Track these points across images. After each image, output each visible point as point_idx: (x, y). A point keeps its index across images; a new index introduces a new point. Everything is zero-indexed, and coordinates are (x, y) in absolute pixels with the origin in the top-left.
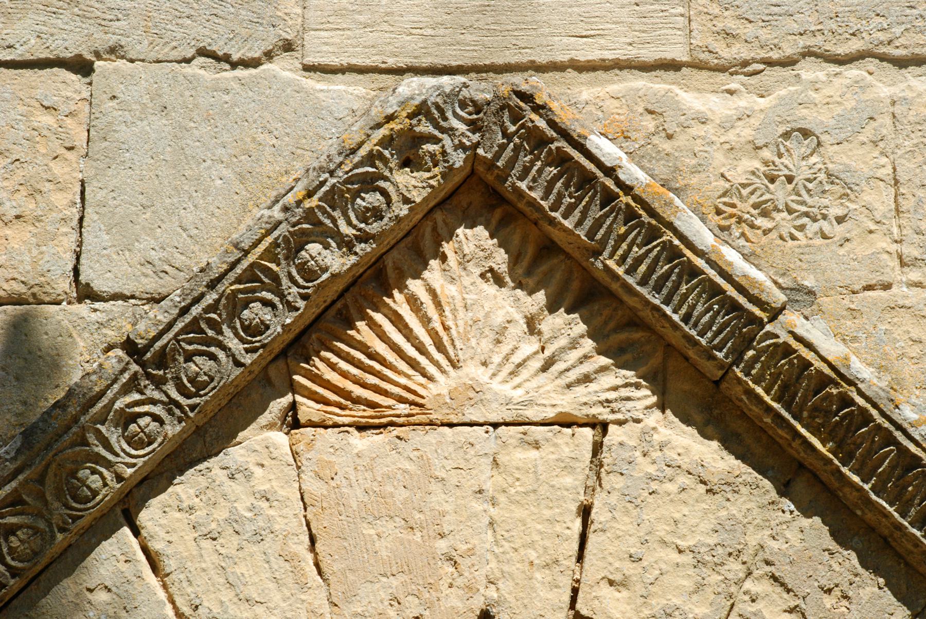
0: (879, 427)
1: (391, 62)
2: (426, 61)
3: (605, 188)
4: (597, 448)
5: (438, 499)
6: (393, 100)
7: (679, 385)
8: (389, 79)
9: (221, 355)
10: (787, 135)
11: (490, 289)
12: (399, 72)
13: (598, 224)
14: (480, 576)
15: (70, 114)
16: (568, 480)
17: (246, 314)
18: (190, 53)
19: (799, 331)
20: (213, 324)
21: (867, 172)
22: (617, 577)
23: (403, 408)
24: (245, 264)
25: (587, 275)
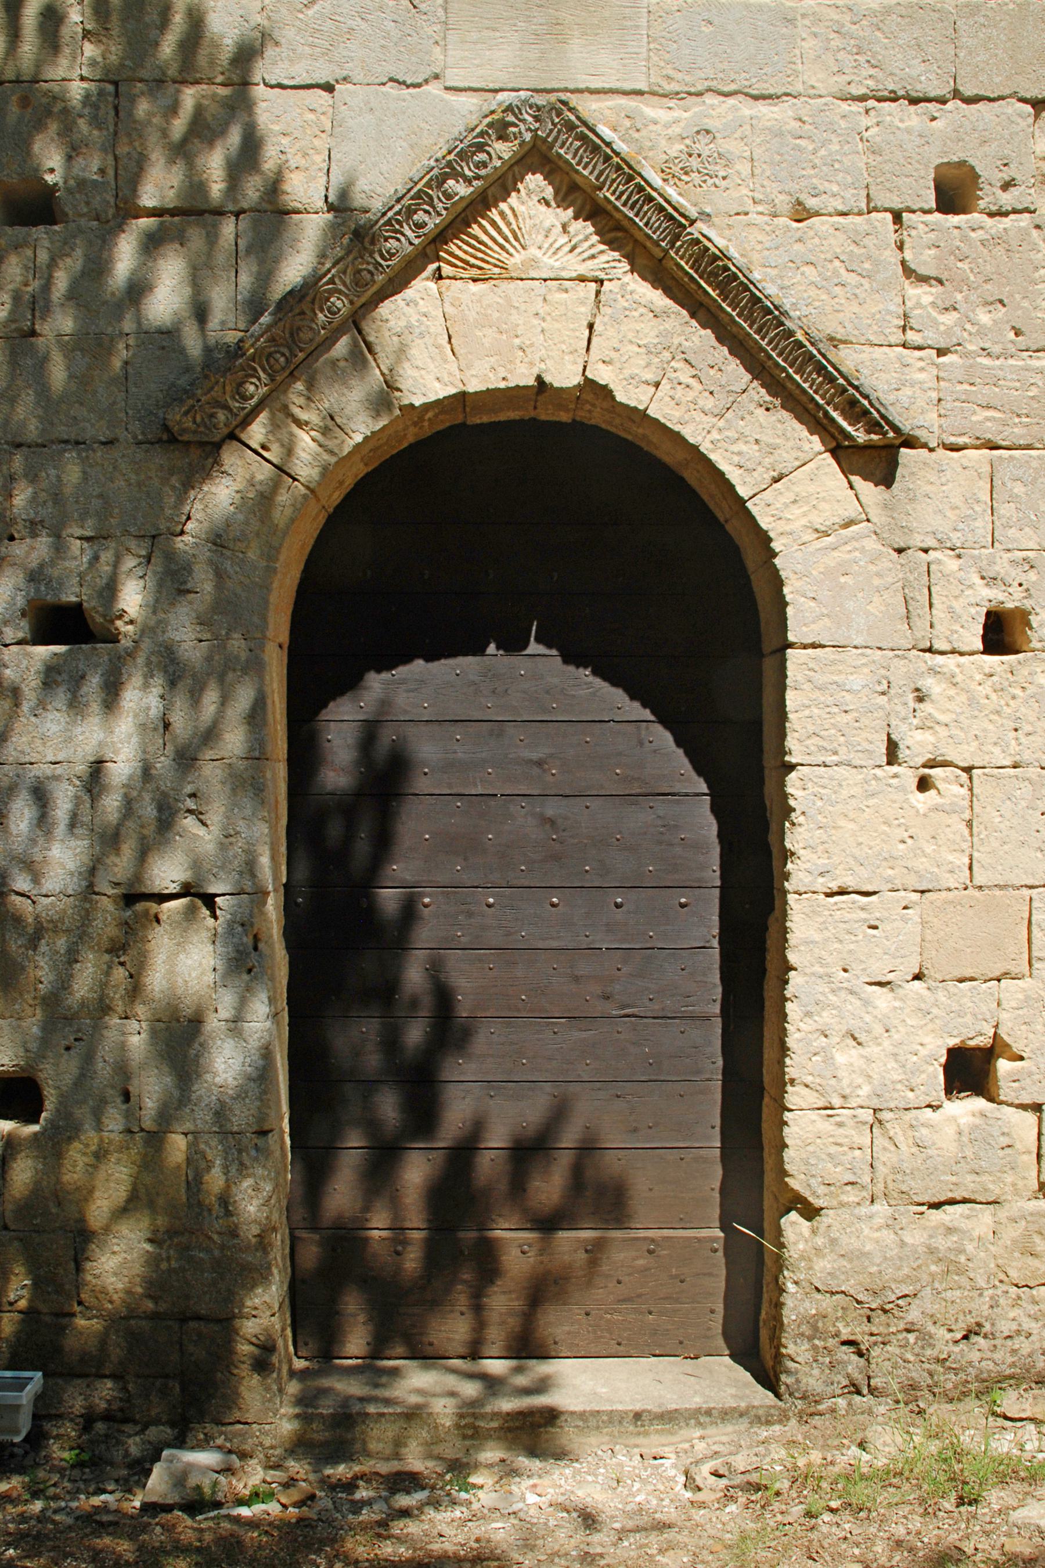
0: (742, 283)
1: (491, 86)
2: (510, 86)
3: (606, 154)
4: (598, 293)
5: (515, 317)
6: (494, 103)
7: (640, 261)
8: (490, 95)
9: (403, 239)
10: (698, 132)
11: (543, 208)
12: (496, 91)
13: (601, 173)
14: (537, 357)
15: (323, 113)
16: (583, 309)
17: (415, 217)
18: (385, 80)
19: (705, 232)
20: (399, 222)
21: (737, 153)
22: (607, 359)
23: (497, 270)
24: (415, 190)
25: (594, 201)
